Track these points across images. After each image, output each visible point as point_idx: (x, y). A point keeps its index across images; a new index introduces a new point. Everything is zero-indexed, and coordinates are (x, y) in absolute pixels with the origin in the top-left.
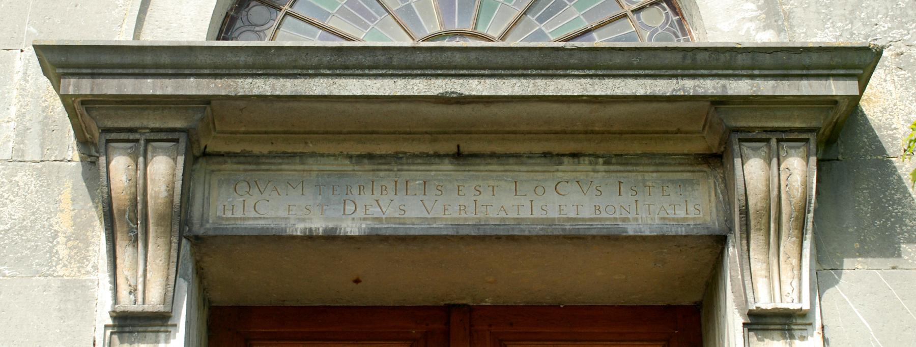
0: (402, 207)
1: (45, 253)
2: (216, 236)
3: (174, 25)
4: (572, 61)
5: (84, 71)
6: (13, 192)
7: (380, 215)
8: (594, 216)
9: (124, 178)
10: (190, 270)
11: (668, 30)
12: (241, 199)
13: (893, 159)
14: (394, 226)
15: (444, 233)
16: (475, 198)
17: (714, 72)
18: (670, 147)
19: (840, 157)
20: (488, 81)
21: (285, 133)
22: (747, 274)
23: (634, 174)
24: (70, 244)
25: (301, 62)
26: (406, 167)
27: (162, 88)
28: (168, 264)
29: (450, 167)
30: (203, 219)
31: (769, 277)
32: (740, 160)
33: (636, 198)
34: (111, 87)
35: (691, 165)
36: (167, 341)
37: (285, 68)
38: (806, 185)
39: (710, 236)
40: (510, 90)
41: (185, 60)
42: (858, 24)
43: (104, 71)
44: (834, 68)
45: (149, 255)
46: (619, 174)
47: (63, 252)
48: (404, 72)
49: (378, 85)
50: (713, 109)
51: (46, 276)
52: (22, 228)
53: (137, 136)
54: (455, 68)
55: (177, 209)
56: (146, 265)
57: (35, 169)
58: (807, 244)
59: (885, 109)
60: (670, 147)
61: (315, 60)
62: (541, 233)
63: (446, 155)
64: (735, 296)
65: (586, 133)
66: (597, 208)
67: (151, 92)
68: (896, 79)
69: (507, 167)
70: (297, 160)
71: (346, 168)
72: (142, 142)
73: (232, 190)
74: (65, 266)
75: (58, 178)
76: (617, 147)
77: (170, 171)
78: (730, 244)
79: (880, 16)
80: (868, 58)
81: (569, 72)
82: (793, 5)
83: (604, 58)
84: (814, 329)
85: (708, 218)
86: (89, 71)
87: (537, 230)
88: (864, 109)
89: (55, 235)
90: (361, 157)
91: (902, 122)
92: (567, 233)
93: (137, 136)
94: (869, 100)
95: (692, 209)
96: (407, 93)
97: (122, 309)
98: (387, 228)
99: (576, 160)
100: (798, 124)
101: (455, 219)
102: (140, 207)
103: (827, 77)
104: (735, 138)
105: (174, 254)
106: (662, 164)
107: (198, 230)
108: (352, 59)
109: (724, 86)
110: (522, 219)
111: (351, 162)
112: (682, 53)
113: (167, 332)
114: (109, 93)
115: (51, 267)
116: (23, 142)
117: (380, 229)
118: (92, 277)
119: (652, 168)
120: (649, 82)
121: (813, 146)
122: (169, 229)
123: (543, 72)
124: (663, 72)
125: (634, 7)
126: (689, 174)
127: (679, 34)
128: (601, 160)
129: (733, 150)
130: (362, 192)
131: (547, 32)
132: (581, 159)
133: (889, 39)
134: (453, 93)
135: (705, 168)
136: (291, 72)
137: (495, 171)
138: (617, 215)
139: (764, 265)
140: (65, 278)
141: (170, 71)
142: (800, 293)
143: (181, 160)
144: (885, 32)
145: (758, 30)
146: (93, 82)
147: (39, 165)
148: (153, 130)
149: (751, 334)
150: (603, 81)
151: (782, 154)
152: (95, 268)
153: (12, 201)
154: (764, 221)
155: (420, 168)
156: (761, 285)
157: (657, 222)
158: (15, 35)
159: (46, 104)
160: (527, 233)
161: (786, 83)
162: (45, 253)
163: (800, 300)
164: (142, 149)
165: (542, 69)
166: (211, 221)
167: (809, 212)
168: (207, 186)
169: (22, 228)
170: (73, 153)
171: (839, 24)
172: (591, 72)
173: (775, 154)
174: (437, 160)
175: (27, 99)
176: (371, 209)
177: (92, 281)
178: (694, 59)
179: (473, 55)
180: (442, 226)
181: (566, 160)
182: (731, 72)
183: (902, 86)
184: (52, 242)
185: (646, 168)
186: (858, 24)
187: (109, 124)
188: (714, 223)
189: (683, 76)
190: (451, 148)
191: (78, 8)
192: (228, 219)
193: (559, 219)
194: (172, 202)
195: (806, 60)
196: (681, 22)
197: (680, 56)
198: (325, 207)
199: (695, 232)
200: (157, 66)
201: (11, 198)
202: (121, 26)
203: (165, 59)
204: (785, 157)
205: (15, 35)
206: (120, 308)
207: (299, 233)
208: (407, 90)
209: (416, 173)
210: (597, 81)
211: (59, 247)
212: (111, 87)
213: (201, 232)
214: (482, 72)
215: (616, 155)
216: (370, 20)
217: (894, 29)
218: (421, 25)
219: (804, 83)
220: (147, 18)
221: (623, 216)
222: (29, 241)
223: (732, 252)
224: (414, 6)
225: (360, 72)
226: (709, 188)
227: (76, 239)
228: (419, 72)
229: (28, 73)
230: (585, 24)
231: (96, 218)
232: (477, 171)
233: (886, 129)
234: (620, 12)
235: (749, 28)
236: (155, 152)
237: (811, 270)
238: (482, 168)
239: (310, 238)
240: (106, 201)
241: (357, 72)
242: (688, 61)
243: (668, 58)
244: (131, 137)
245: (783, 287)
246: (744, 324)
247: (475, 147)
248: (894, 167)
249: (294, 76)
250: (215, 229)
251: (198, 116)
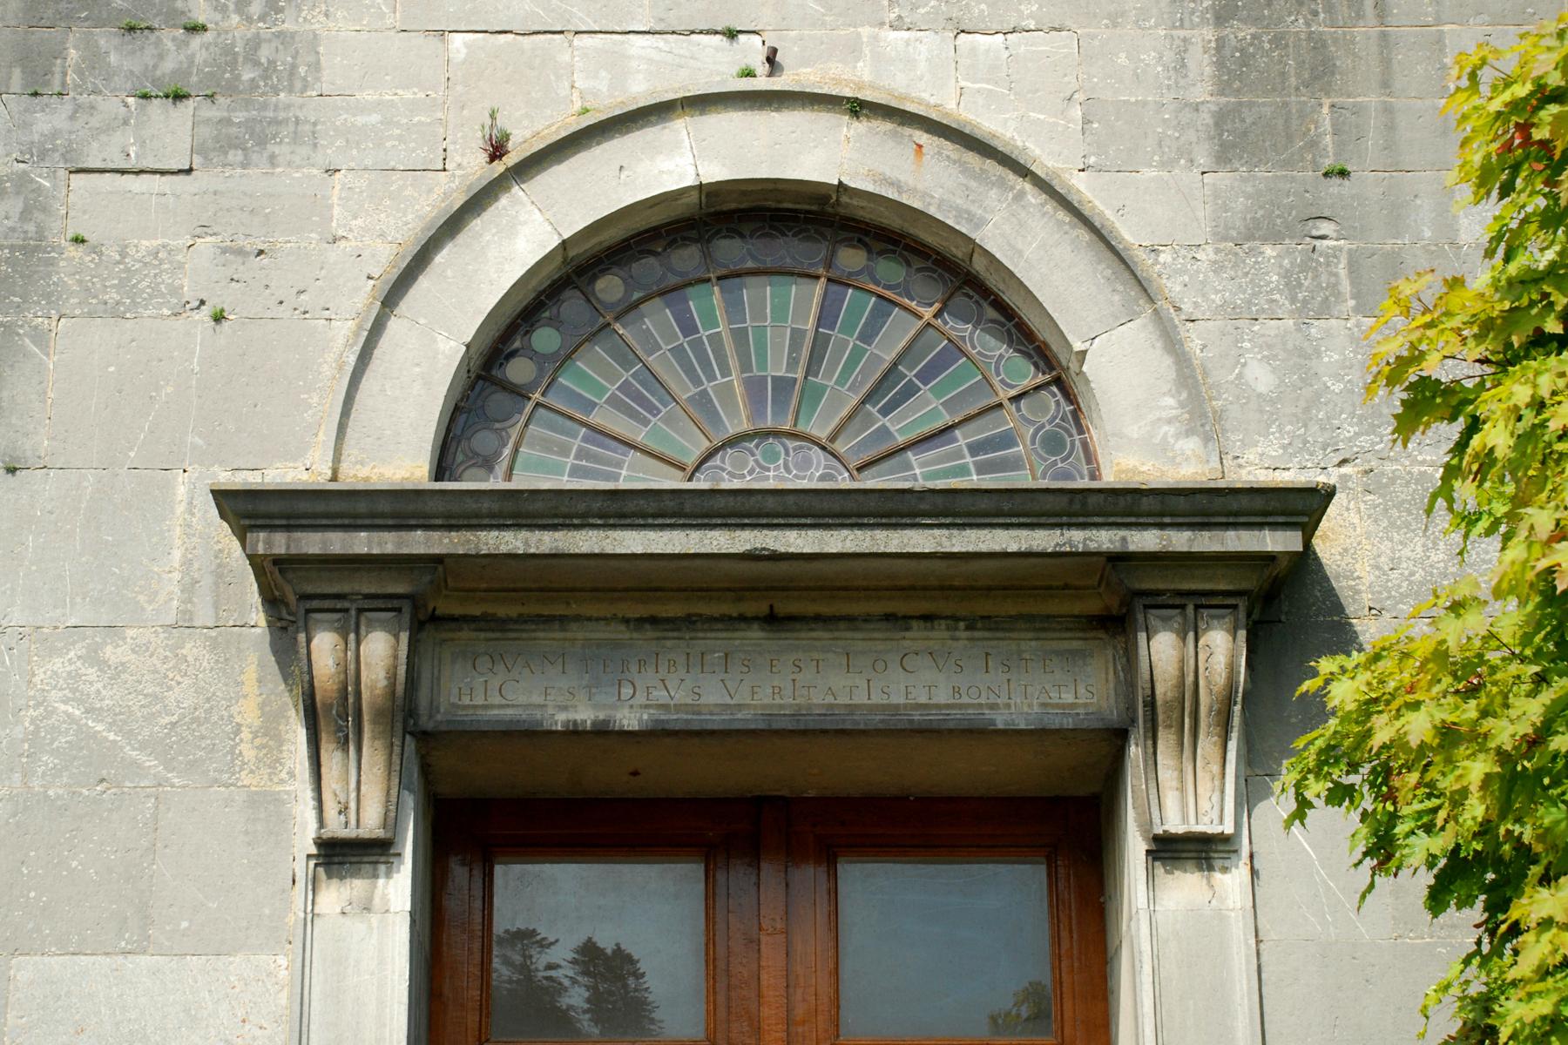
0: (696, 690)
1: (225, 755)
3: (388, 432)
4: (922, 507)
5: (277, 522)
6: (180, 671)
8: (952, 701)
9: (331, 662)
10: (416, 775)
11: (1058, 426)
13: (1354, 621)
14: (685, 717)
15: (753, 727)
16: (793, 677)
17: (1111, 520)
18: (1053, 607)
19: (1283, 618)
20: (811, 533)
21: (541, 590)
22: (1152, 785)
23: (1005, 643)
24: (258, 742)
25: (564, 510)
26: (701, 635)
27: (380, 544)
28: (390, 773)
30: (433, 708)
31: (1182, 789)
33: (1007, 676)
34: (312, 543)
35: (1083, 630)
36: (388, 875)
37: (542, 516)
40: (840, 545)
41: (411, 507)
42: (1314, 428)
43: (304, 522)
45: (364, 761)
46: (985, 643)
47: (249, 752)
48: (700, 521)
50: (1110, 565)
51: (227, 786)
52: (194, 720)
53: (346, 605)
54: (767, 515)
55: (399, 702)
56: (359, 775)
58: (1233, 745)
59: (1346, 550)
60: (1053, 607)
61: (581, 507)
62: (881, 726)
63: (756, 618)
64: (1137, 814)
65: (942, 588)
66: (956, 691)
67: (365, 550)
68: (1362, 506)
69: (837, 634)
70: (557, 625)
71: (620, 636)
72: (353, 613)
73: (469, 666)
74: (252, 772)
75: (239, 650)
76: (984, 607)
77: (390, 652)
78: (1132, 742)
79: (1344, 416)
80: (1315, 502)
81: (918, 520)
82: (1226, 399)
83: (963, 503)
84: (1239, 859)
85: (1104, 705)
86: (284, 522)
87: (876, 720)
88: (1318, 550)
89: (237, 732)
90: (641, 621)
91: (1368, 569)
92: (916, 726)
93: (346, 605)
94: (1325, 537)
95: (1083, 691)
97: (330, 835)
98: (675, 719)
99: (929, 624)
101: (764, 706)
102: (351, 700)
103: (1260, 526)
104: (1139, 604)
105: (396, 759)
106: (1044, 630)
107: (426, 723)
108: (631, 506)
109: (1124, 539)
110: (856, 706)
111: (628, 627)
112: (1069, 496)
113: (388, 863)
114: (311, 552)
115: (233, 774)
117: (668, 721)
119: (1030, 635)
120: (1024, 533)
121: (1242, 615)
122: (389, 728)
123: (884, 521)
124: (1043, 520)
125: (1013, 393)
126: (1080, 642)
127: (1074, 431)
128: (962, 625)
129: (1136, 620)
130: (643, 670)
131: (892, 429)
132: (936, 622)
133: (1355, 449)
134: (764, 549)
135: (1101, 634)
136: (550, 522)
137: (819, 639)
138: (983, 701)
139: (1176, 774)
140: (253, 789)
141: (390, 522)
142: (1222, 810)
143: (404, 637)
144: (1350, 439)
145: (1177, 436)
146: (289, 538)
147: (213, 633)
148: (368, 597)
149: (1157, 864)
150: (964, 533)
151: (1202, 625)
152: (291, 774)
153: (179, 683)
154: (1175, 715)
155: (720, 635)
157: (1036, 709)
158: (175, 448)
159: (220, 546)
160: (862, 727)
161: (1206, 534)
162: (225, 755)
163: (1221, 821)
164: (353, 622)
165: (882, 516)
166: (442, 710)
167: (1235, 704)
168: (436, 662)
169: (194, 720)
170: (258, 617)
171: (1289, 428)
172: (948, 521)
173: (1192, 625)
174: (743, 625)
175: (194, 539)
176: (655, 693)
177: (287, 793)
178: (1084, 504)
179: (791, 499)
180: (749, 717)
181: (914, 623)
182: (1133, 520)
183: (1369, 517)
184: (233, 740)
185: (1022, 635)
186: (1314, 428)
187: (310, 589)
188: (1112, 712)
189: (1070, 526)
190: (762, 608)
192: (466, 707)
193: (905, 706)
194: (393, 693)
196: (1076, 414)
197: (1065, 499)
198: (594, 690)
200: (373, 516)
201: (178, 678)
204: (1206, 630)
205: (175, 448)
206: (327, 833)
207: (559, 728)
208: (704, 546)
209: (715, 643)
210: (955, 532)
211: (243, 747)
212: (312, 543)
214: (803, 521)
215: (983, 618)
216: (650, 412)
217: (1363, 434)
218: (722, 421)
219: (1231, 534)
221: (991, 701)
223: (1135, 752)
224: (711, 393)
226: (1107, 662)
227: (265, 735)
228: (719, 521)
229: (195, 502)
230: (946, 419)
231: (291, 706)
232: (798, 639)
233: (1346, 578)
234: (993, 400)
235: (1166, 433)
236: (371, 627)
237: (1237, 777)
238: (803, 635)
239: (574, 733)
240: (307, 692)
241: (637, 522)
243: (1050, 503)
244: (339, 606)
245: (1199, 802)
246: (1147, 851)
248: (1355, 632)
249: (554, 527)
250: (449, 722)
251: (427, 578)
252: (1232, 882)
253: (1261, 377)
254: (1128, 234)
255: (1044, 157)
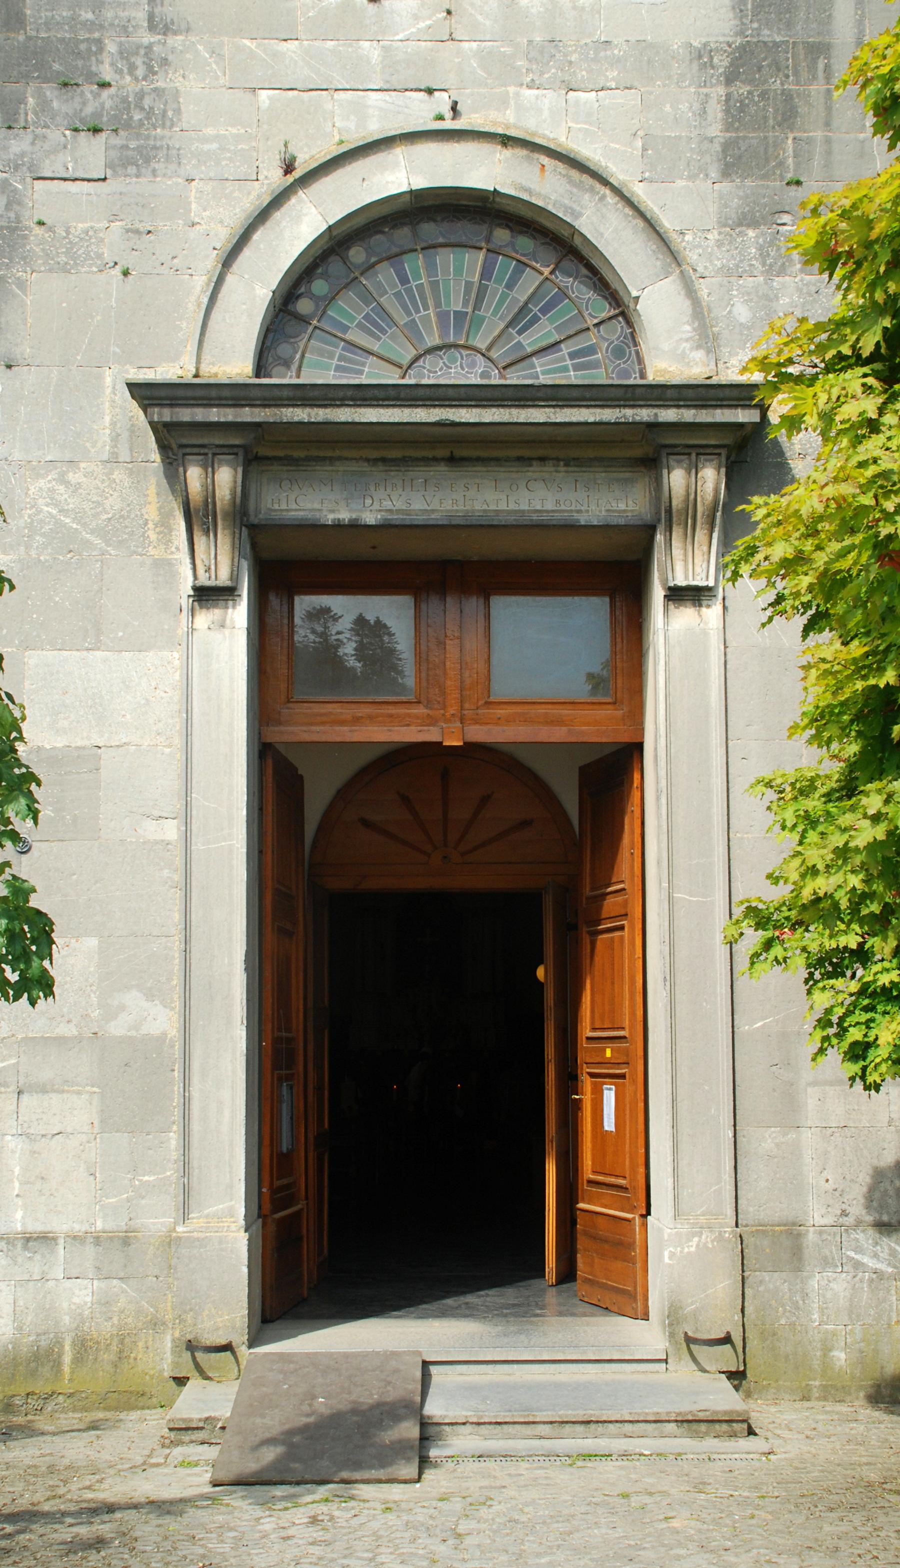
2: (266, 525)
5: (165, 402)
7: (391, 507)
10: (248, 550)
11: (622, 342)
12: (285, 494)
17: (649, 403)
18: (617, 453)
19: (748, 460)
20: (474, 410)
24: (158, 530)
25: (330, 396)
26: (411, 469)
27: (224, 416)
29: (446, 468)
30: (257, 511)
31: (685, 561)
32: (666, 471)
33: (587, 494)
34: (186, 415)
36: (234, 607)
37: (318, 399)
38: (717, 490)
39: (644, 525)
43: (180, 402)
44: (742, 400)
45: (218, 542)
47: (153, 536)
49: (389, 413)
51: (141, 555)
53: (206, 451)
54: (449, 400)
55: (238, 508)
56: (216, 550)
57: (127, 469)
58: (715, 535)
60: (617, 453)
61: (341, 394)
63: (443, 459)
66: (558, 502)
69: (490, 468)
71: (364, 469)
72: (210, 455)
73: (278, 486)
74: (155, 547)
77: (232, 479)
78: (658, 533)
81: (536, 403)
84: (717, 600)
85: (643, 511)
86: (168, 402)
87: (511, 519)
88: (771, 419)
89: (146, 524)
96: (412, 420)
97: (200, 584)
100: (713, 442)
102: (210, 507)
103: (736, 406)
104: (664, 452)
105: (237, 541)
107: (254, 520)
109: (656, 415)
116: (116, 446)
118: (176, 557)
119: (602, 469)
120: (598, 410)
121: (723, 459)
123: (517, 403)
124: (609, 403)
125: (596, 321)
127: (631, 345)
128: (562, 463)
129: (662, 462)
131: (524, 343)
136: (323, 403)
138: (573, 508)
139: (682, 552)
141: (230, 403)
143: (240, 470)
145: (691, 349)
147: (130, 466)
148: (218, 446)
151: (700, 465)
152: (178, 549)
155: (422, 469)
156: (679, 567)
157: (604, 513)
159: (132, 414)
160: (503, 523)
161: (704, 411)
164: (210, 461)
165: (515, 400)
170: (156, 456)
172: (554, 403)
175: (117, 410)
177: (176, 559)
182: (661, 403)
185: (597, 469)
187: (185, 441)
189: (625, 406)
191: (151, 330)
193: (528, 511)
195: (720, 393)
196: (633, 335)
197: (622, 391)
199: (631, 523)
200: (220, 399)
201: (111, 492)
202: (186, 347)
203: (226, 393)
204: (703, 468)
209: (419, 473)
210: (558, 410)
213: (256, 522)
214: (470, 403)
219: (718, 411)
220: (206, 340)
221: (578, 508)
222: (126, 527)
223: (659, 538)
225: (376, 403)
227: (162, 526)
228: (421, 403)
230: (556, 337)
234: (585, 326)
236: (220, 464)
238: (470, 469)
239: (338, 526)
242: (629, 395)
243: (614, 393)
244: (202, 452)
247: (465, 453)
249: (325, 406)
250: (267, 519)
252: (712, 613)
253: (742, 313)
254: (668, 223)
255: (618, 173)
